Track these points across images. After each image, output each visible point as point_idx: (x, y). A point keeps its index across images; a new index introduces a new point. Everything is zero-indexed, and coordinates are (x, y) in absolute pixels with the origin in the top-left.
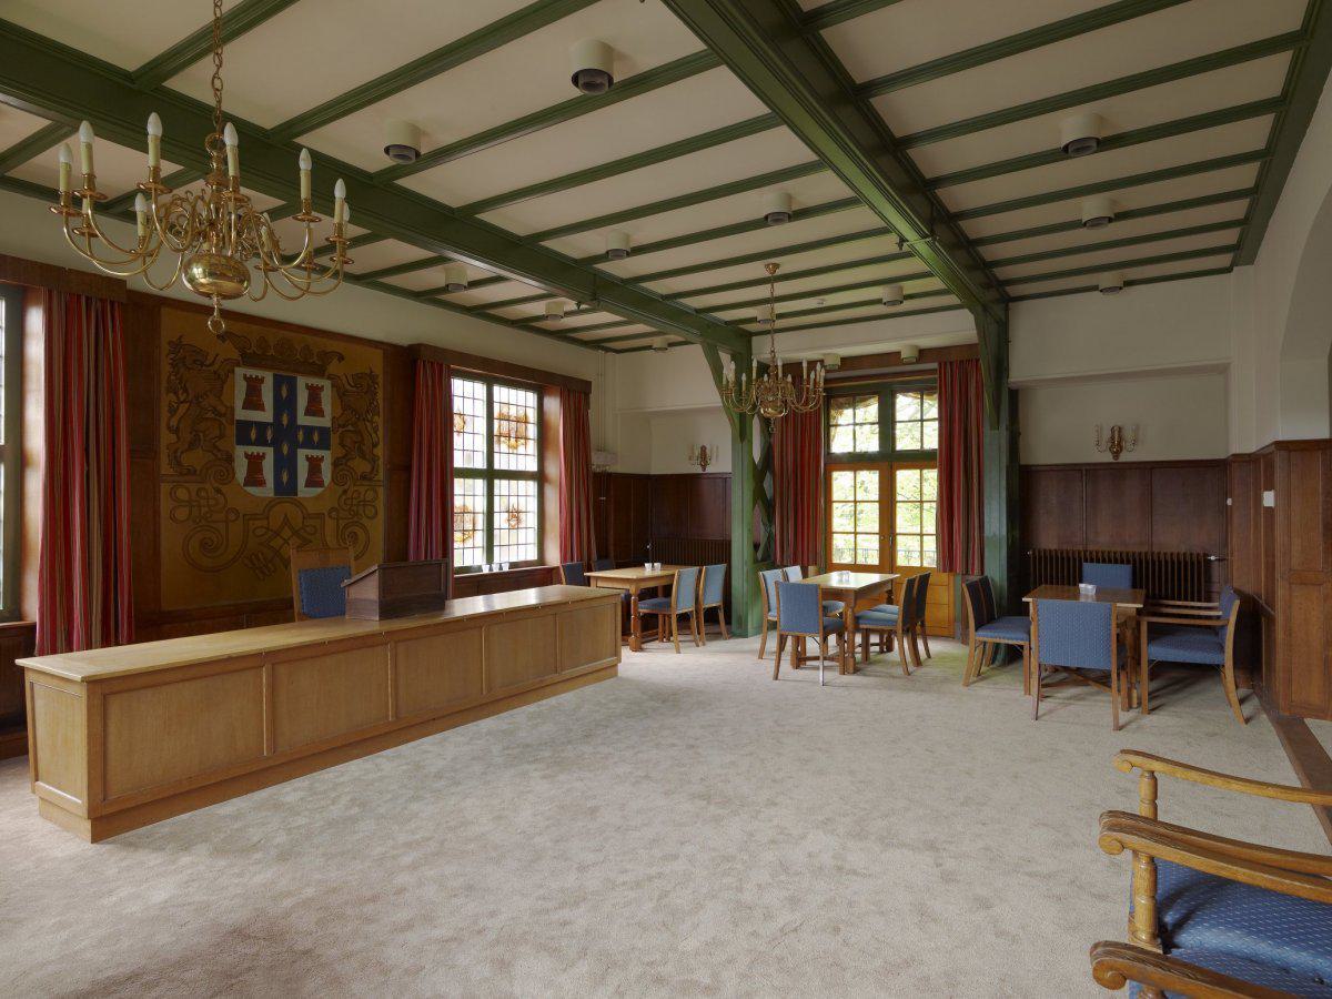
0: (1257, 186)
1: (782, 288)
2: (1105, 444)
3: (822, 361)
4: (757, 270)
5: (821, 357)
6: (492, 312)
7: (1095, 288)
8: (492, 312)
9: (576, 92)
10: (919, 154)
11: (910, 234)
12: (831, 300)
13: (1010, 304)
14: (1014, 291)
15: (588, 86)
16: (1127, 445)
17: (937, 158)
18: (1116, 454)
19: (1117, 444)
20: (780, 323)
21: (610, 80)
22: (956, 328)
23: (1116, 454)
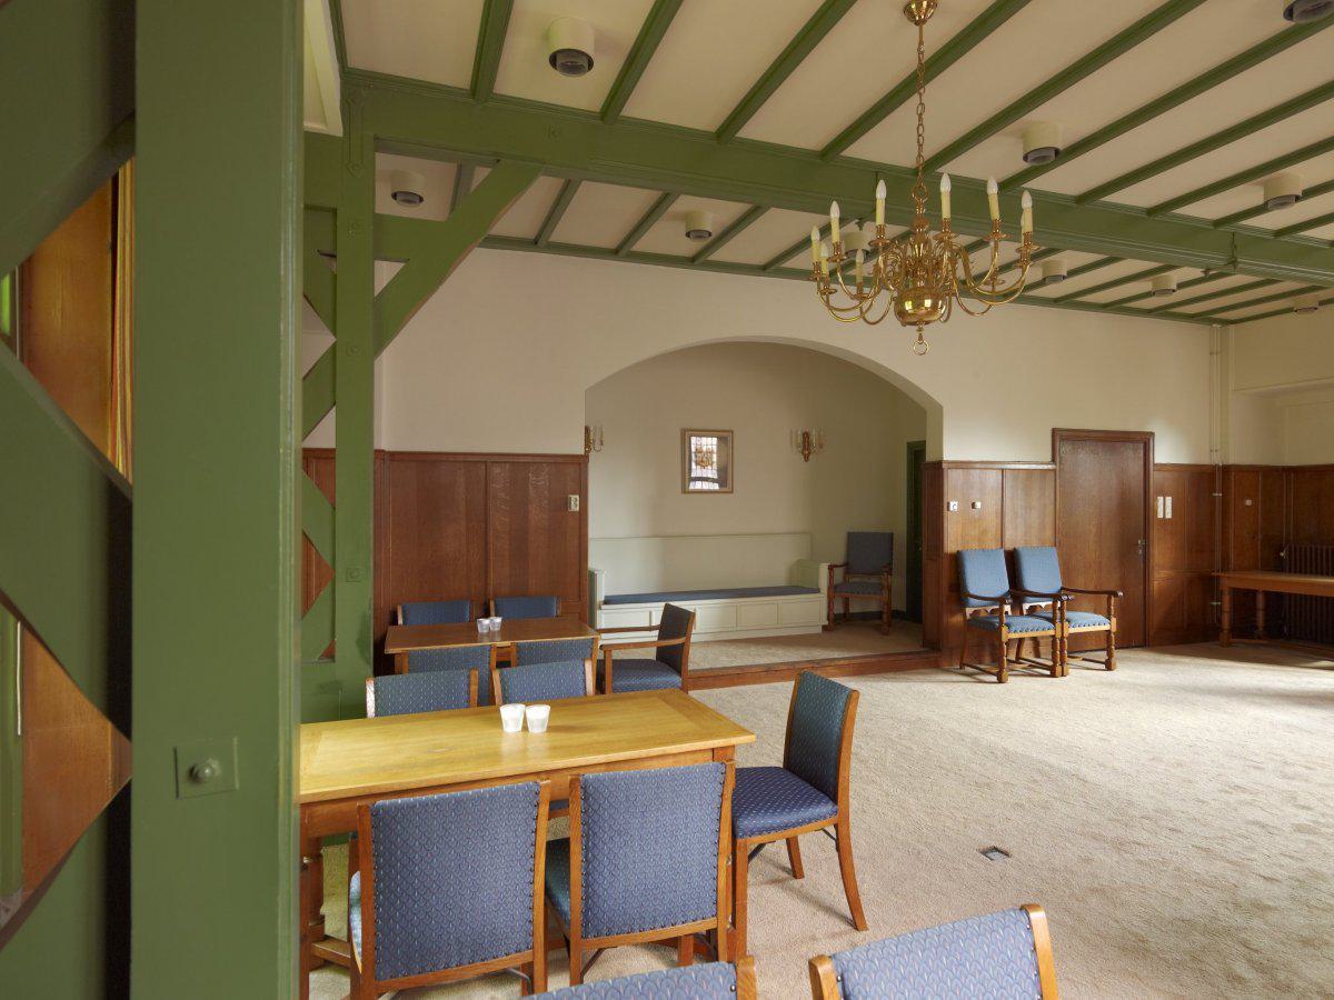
6: (1079, 299)
8: (1079, 299)
9: (1287, 24)
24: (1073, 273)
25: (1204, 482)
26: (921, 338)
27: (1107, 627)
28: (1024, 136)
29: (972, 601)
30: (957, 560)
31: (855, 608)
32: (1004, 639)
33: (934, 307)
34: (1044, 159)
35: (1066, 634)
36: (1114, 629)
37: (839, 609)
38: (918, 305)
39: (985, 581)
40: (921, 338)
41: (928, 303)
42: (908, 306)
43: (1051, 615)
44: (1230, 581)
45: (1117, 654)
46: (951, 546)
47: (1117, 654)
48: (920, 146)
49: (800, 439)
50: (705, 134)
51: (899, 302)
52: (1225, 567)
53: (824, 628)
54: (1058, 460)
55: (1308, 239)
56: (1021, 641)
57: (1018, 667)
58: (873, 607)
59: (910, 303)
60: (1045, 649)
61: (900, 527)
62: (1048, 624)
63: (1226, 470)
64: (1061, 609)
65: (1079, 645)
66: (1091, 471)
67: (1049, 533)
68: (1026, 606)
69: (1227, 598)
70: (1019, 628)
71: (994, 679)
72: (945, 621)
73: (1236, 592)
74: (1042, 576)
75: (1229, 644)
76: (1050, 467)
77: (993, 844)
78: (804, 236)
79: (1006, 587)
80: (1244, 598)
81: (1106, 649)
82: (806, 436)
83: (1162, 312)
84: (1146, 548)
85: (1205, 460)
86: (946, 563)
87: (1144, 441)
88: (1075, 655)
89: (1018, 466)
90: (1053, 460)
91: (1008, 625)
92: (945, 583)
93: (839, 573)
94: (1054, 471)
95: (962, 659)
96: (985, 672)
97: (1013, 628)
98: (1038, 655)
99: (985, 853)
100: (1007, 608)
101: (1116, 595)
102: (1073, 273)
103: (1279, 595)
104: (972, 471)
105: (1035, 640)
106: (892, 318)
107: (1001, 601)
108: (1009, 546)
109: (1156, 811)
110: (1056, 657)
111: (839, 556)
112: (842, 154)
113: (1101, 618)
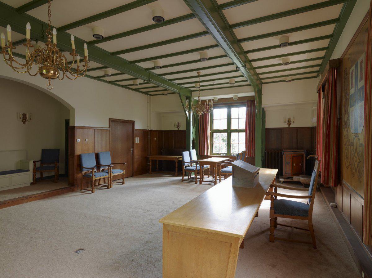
0: (325, 56)
1: (202, 79)
2: (287, 123)
3: (213, 100)
4: (195, 73)
5: (213, 98)
6: (129, 87)
7: (284, 81)
8: (129, 87)
9: (154, 23)
10: (236, 31)
11: (239, 65)
12: (216, 82)
13: (263, 85)
14: (264, 81)
15: (157, 21)
16: (292, 123)
17: (241, 33)
18: (289, 125)
19: (289, 122)
20: (201, 88)
21: (164, 19)
22: (249, 93)
23: (289, 125)
24: (113, 75)
25: (146, 134)
26: (49, 83)
27: (122, 173)
28: (93, 29)
29: (84, 169)
30: (80, 157)
31: (45, 175)
32: (94, 180)
33: (54, 73)
34: (101, 39)
35: (112, 176)
36: (124, 173)
37: (38, 176)
38: (48, 72)
39: (89, 163)
40: (49, 83)
41: (52, 72)
42: (44, 72)
43: (107, 171)
44: (151, 158)
45: (125, 180)
46: (78, 152)
47: (125, 180)
48: (49, 17)
49: (21, 116)
50: (11, 8)
51: (41, 69)
52: (150, 155)
53: (32, 183)
54: (110, 127)
55: (174, 82)
56: (100, 179)
57: (98, 187)
58: (52, 174)
59: (45, 71)
60: (107, 181)
61: (63, 147)
62: (107, 174)
63: (151, 131)
64: (110, 169)
65: (115, 179)
66: (120, 131)
67: (108, 147)
68: (101, 169)
69: (150, 162)
70: (98, 175)
71: (91, 192)
72: (76, 176)
73: (153, 161)
74: (106, 160)
75: (151, 174)
76: (108, 129)
77: (79, 248)
78: (71, 61)
79: (95, 164)
80: (154, 162)
81: (122, 178)
82: (24, 115)
83: (136, 90)
84: (133, 151)
85: (146, 128)
86: (76, 158)
87: (133, 123)
88: (115, 181)
89: (104, 129)
90: (109, 127)
91: (95, 176)
92: (76, 164)
93: (38, 164)
94: (110, 130)
95: (81, 187)
96: (88, 190)
97: (96, 176)
98: (105, 183)
99: (76, 252)
100: (96, 170)
101: (125, 164)
102: (113, 75)
103: (161, 161)
104: (84, 129)
105: (104, 179)
106: (38, 74)
107: (93, 168)
108: (96, 152)
109: (128, 223)
110: (108, 183)
111: (38, 157)
112: (26, 13)
113: (121, 170)
